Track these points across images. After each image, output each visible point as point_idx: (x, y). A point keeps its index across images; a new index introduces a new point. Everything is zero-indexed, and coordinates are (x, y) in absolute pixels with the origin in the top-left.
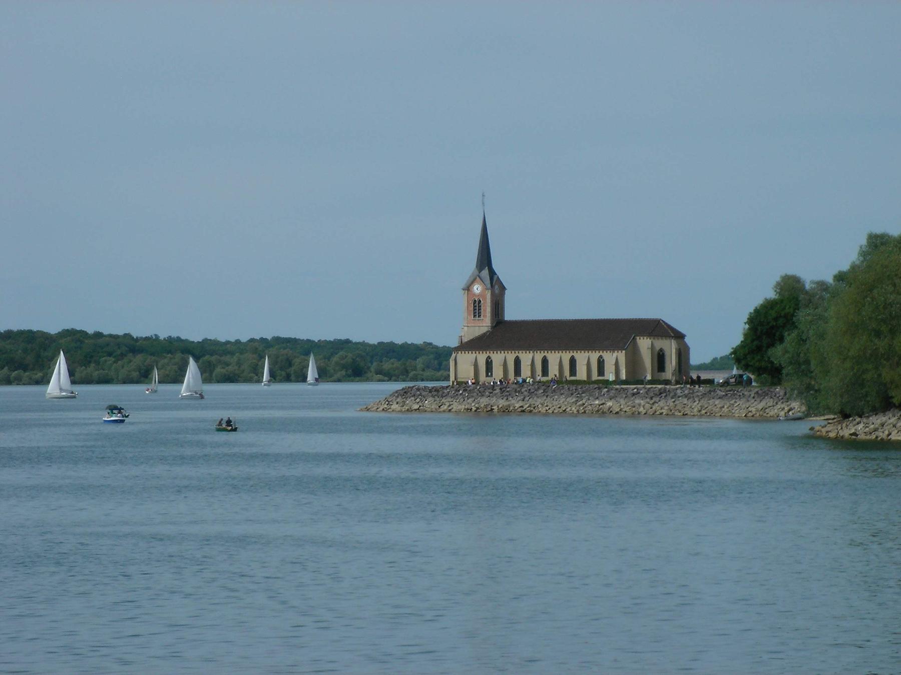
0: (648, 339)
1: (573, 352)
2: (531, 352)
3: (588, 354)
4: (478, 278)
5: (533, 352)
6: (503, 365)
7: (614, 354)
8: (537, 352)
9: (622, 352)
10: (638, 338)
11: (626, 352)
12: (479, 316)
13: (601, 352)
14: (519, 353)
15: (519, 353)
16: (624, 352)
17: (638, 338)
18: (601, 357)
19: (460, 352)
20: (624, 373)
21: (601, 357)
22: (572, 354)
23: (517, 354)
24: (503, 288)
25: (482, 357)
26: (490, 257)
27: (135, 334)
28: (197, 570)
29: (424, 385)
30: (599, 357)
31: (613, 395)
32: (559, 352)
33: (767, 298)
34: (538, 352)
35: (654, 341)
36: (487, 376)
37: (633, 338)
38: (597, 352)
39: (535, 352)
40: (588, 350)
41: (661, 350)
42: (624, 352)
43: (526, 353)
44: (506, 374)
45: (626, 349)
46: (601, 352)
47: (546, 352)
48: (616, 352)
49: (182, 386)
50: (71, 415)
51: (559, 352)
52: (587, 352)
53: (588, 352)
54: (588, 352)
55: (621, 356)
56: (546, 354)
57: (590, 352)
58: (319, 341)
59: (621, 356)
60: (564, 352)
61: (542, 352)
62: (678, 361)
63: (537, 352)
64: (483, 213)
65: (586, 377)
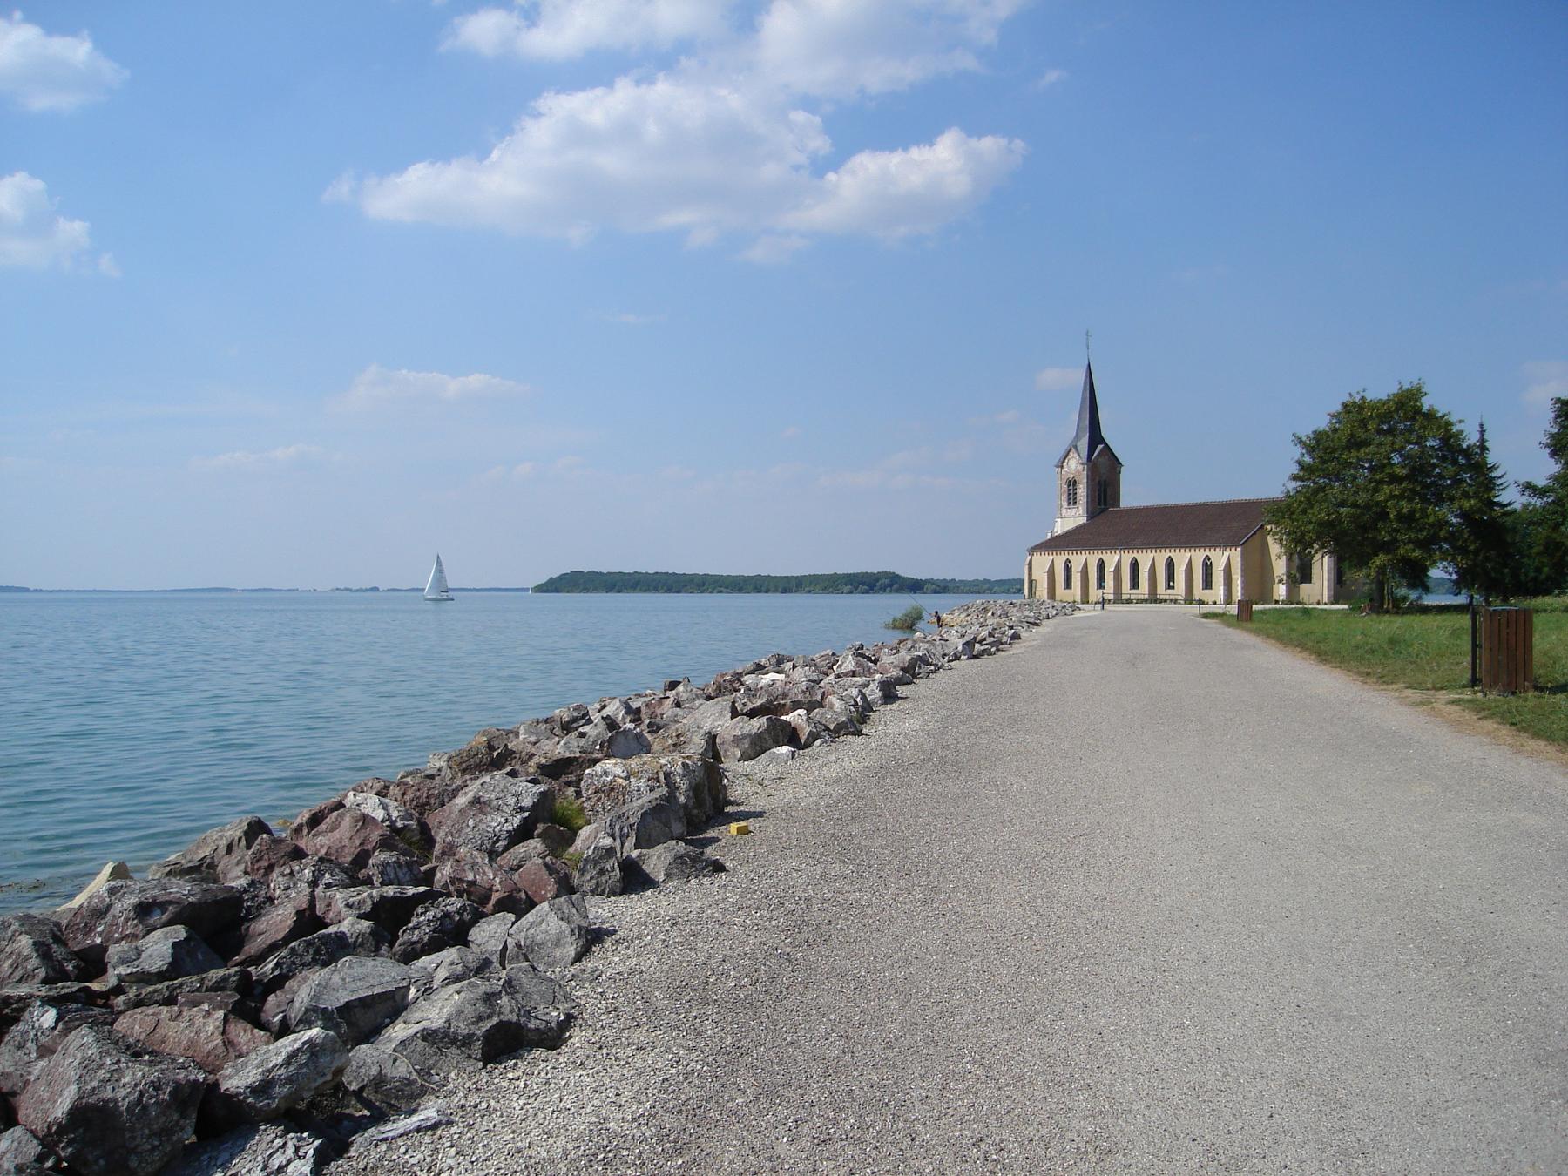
4: (1073, 450)
5: (1120, 552)
12: (1075, 503)
16: (1239, 549)
18: (1208, 558)
20: (1239, 582)
21: (1208, 558)
23: (1100, 556)
24: (1115, 464)
25: (1060, 560)
27: (554, 576)
31: (202, 1158)
33: (927, 148)
34: (1126, 551)
42: (1239, 549)
44: (1101, 572)
46: (1207, 550)
48: (1228, 549)
50: (178, 743)
52: (1202, 550)
55: (1236, 555)
57: (1193, 550)
58: (1555, 452)
59: (1236, 555)
60: (1158, 551)
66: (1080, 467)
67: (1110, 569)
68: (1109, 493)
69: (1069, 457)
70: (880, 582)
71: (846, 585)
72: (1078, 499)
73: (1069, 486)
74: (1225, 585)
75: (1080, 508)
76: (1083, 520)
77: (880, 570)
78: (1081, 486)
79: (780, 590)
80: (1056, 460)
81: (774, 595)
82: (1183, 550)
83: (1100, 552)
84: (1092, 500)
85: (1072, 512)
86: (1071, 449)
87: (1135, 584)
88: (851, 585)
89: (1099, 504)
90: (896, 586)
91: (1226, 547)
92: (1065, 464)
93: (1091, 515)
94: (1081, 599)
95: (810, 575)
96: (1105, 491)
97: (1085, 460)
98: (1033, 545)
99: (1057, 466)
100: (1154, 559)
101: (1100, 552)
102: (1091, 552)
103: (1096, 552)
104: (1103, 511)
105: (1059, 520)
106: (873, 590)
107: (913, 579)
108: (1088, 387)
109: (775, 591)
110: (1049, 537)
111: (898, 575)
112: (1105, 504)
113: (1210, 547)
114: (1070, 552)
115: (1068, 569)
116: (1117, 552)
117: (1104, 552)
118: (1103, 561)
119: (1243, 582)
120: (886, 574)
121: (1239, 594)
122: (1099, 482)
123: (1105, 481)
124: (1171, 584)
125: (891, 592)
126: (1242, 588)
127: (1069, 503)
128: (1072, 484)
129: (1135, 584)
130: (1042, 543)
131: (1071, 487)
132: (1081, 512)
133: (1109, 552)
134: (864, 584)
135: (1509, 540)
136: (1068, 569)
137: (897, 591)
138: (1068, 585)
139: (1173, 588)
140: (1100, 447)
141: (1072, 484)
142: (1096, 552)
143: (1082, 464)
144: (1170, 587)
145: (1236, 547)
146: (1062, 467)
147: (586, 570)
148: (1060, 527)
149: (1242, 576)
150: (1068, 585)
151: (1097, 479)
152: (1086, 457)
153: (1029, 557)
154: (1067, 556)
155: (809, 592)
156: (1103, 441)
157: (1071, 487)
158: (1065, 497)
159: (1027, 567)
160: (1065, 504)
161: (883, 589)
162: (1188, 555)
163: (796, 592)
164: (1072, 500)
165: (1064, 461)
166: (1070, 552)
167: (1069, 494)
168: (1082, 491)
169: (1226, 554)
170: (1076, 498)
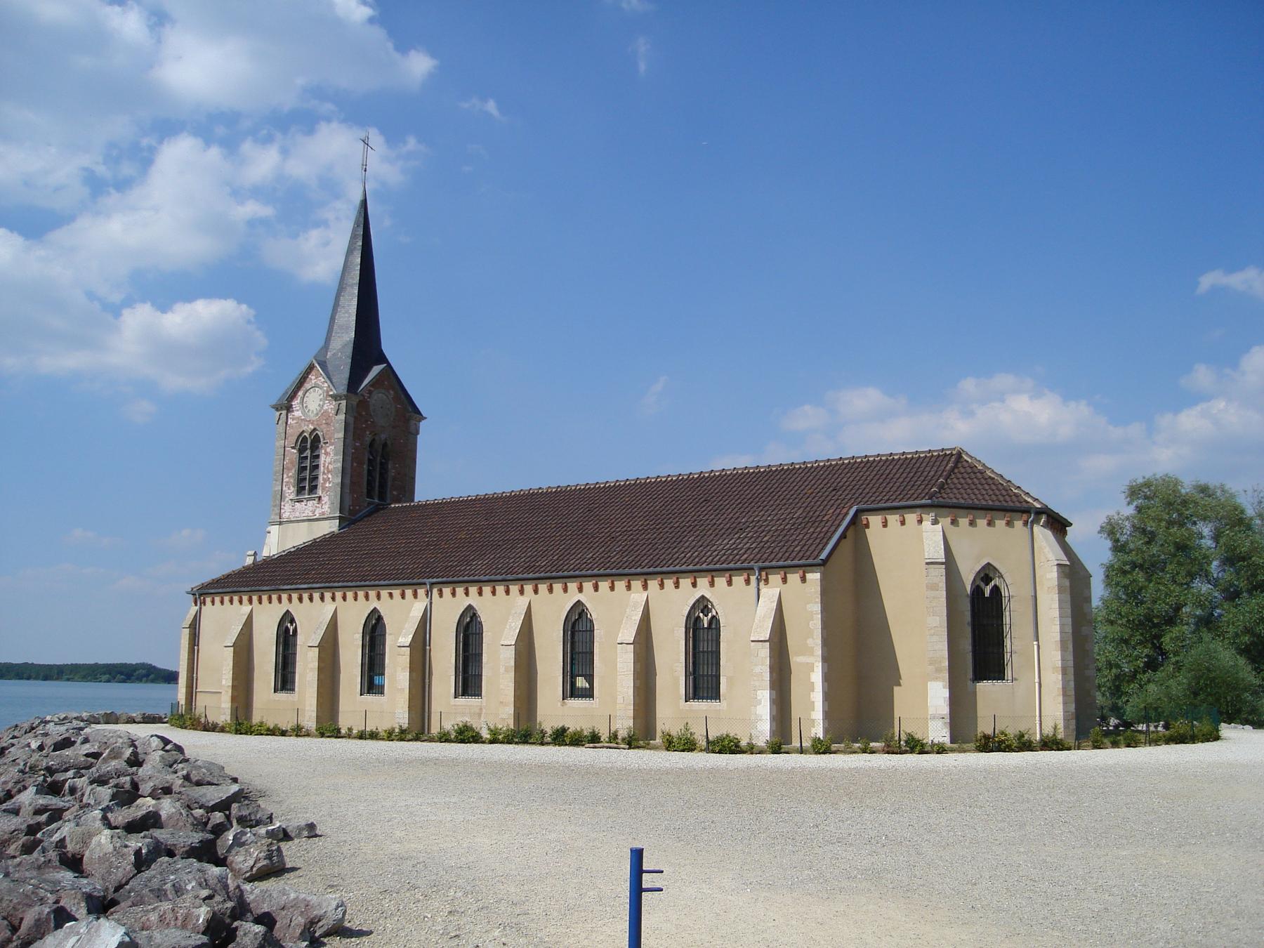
0: (927, 524)
1: (580, 589)
2: (421, 592)
3: (645, 595)
6: (320, 646)
7: (764, 590)
8: (441, 595)
9: (803, 579)
10: (875, 520)
11: (823, 580)
12: (313, 489)
13: (703, 582)
14: (379, 597)
15: (379, 597)
16: (814, 577)
17: (875, 520)
18: (703, 605)
19: (208, 600)
20: (817, 677)
21: (703, 605)
22: (573, 596)
23: (374, 604)
25: (267, 616)
26: (396, 375)
28: (188, 920)
29: (102, 712)
30: (693, 607)
32: (522, 592)
35: (953, 532)
36: (572, 691)
37: (854, 521)
38: (686, 582)
39: (435, 591)
40: (646, 576)
41: (987, 574)
42: (814, 577)
43: (403, 596)
45: (824, 563)
47: (473, 590)
49: (177, 689)
51: (522, 592)
53: (645, 587)
54: (645, 587)
56: (473, 599)
57: (653, 584)
60: (543, 587)
61: (460, 591)
62: (1069, 629)
63: (441, 595)
64: (363, 188)
65: (510, 710)
66: (330, 406)
67: (398, 639)
68: (392, 473)
69: (307, 386)
70: (137, 672)
71: (105, 674)
72: (321, 478)
73: (301, 451)
74: (773, 686)
75: (325, 499)
76: (331, 527)
77: (139, 662)
78: (330, 449)
79: (41, 678)
80: (277, 394)
81: (37, 682)
82: (620, 585)
83: (372, 594)
84: (352, 483)
85: (307, 508)
86: (311, 368)
87: (469, 682)
88: (110, 674)
89: (369, 495)
90: (152, 676)
91: (766, 571)
92: (295, 403)
93: (349, 517)
94: (319, 719)
95: (72, 664)
96: (383, 466)
97: (343, 389)
98: (207, 579)
99: (277, 408)
100: (530, 603)
101: (372, 594)
102: (350, 595)
103: (361, 594)
104: (377, 509)
105: (274, 530)
106: (130, 679)
107: (169, 670)
108: (358, 260)
109: (36, 678)
110: (249, 561)
111: (154, 666)
112: (382, 497)
113: (713, 572)
114: (295, 596)
115: (286, 639)
116: (421, 592)
117: (384, 593)
118: (380, 618)
119: (826, 678)
120: (143, 666)
121: (818, 714)
122: (371, 445)
123: (385, 445)
124: (581, 682)
125: (146, 682)
126: (827, 697)
127: (300, 490)
128: (309, 445)
129: (469, 682)
130: (229, 576)
131: (308, 453)
132: (326, 508)
133: (397, 593)
134: (121, 673)
135: (1188, 578)
136: (286, 639)
137: (153, 681)
138: (285, 680)
139: (588, 694)
140: (376, 370)
141: (309, 445)
142: (361, 594)
143: (335, 397)
144: (572, 691)
145: (806, 567)
146: (289, 409)
147: (134, 663)
148: (275, 543)
149: (825, 659)
150: (285, 680)
151: (368, 439)
152: (346, 382)
153: (194, 609)
154: (285, 606)
155: (68, 680)
156: (382, 358)
157: (308, 453)
158: (290, 476)
159: (186, 634)
160: (290, 492)
161: (139, 679)
162: (637, 596)
163: (57, 679)
164: (307, 484)
165: (293, 396)
166: (295, 596)
167: (302, 469)
168: (330, 460)
169: (770, 592)
170: (316, 478)
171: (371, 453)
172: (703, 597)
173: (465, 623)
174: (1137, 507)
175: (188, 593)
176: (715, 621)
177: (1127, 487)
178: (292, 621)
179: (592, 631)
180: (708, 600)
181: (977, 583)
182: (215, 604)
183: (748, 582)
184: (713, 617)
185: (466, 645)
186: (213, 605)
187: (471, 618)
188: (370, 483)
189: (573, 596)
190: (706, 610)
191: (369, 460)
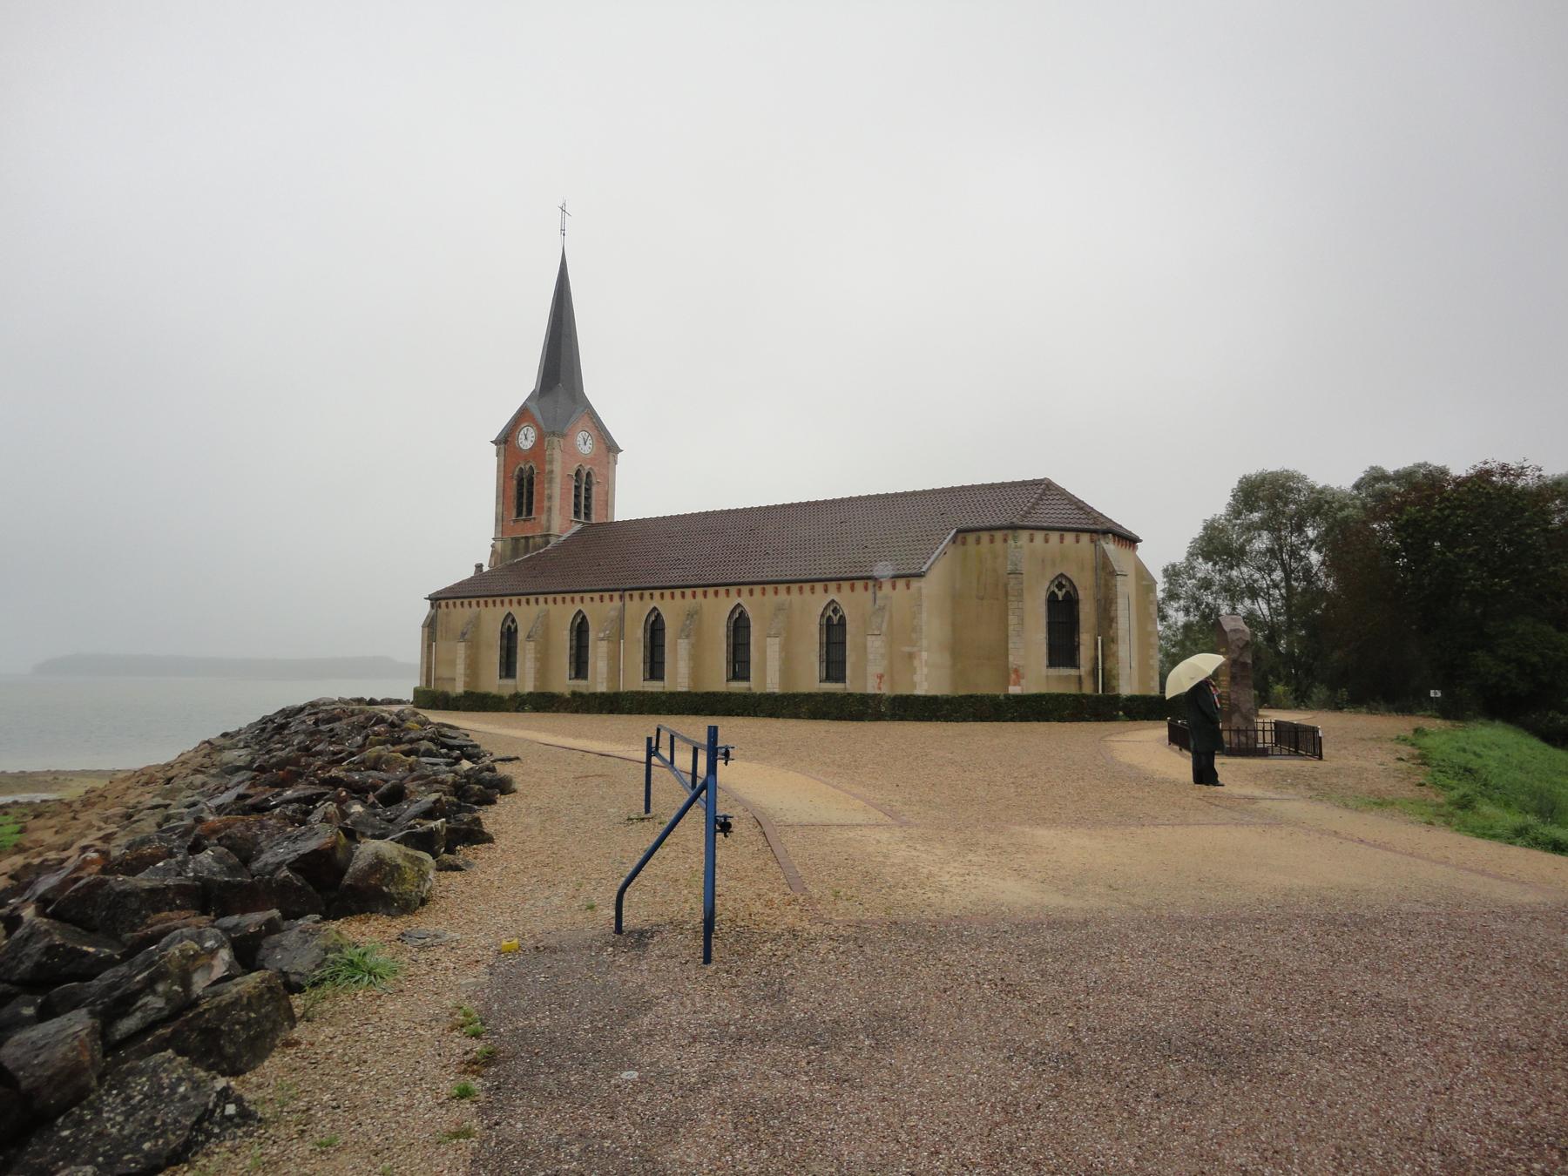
15: (582, 599)
21: (833, 606)
22: (507, 609)
89: (577, 513)
171: (576, 481)
172: (833, 601)
173: (651, 621)
174: (398, 867)
175: (426, 599)
176: (842, 618)
177: (300, 1031)
178: (513, 621)
179: (749, 627)
180: (837, 603)
181: (1052, 589)
182: (731, 595)
183: (866, 588)
184: (841, 616)
185: (653, 637)
186: (602, 601)
187: (656, 617)
188: (577, 505)
189: (507, 609)
190: (835, 611)
191: (575, 486)
